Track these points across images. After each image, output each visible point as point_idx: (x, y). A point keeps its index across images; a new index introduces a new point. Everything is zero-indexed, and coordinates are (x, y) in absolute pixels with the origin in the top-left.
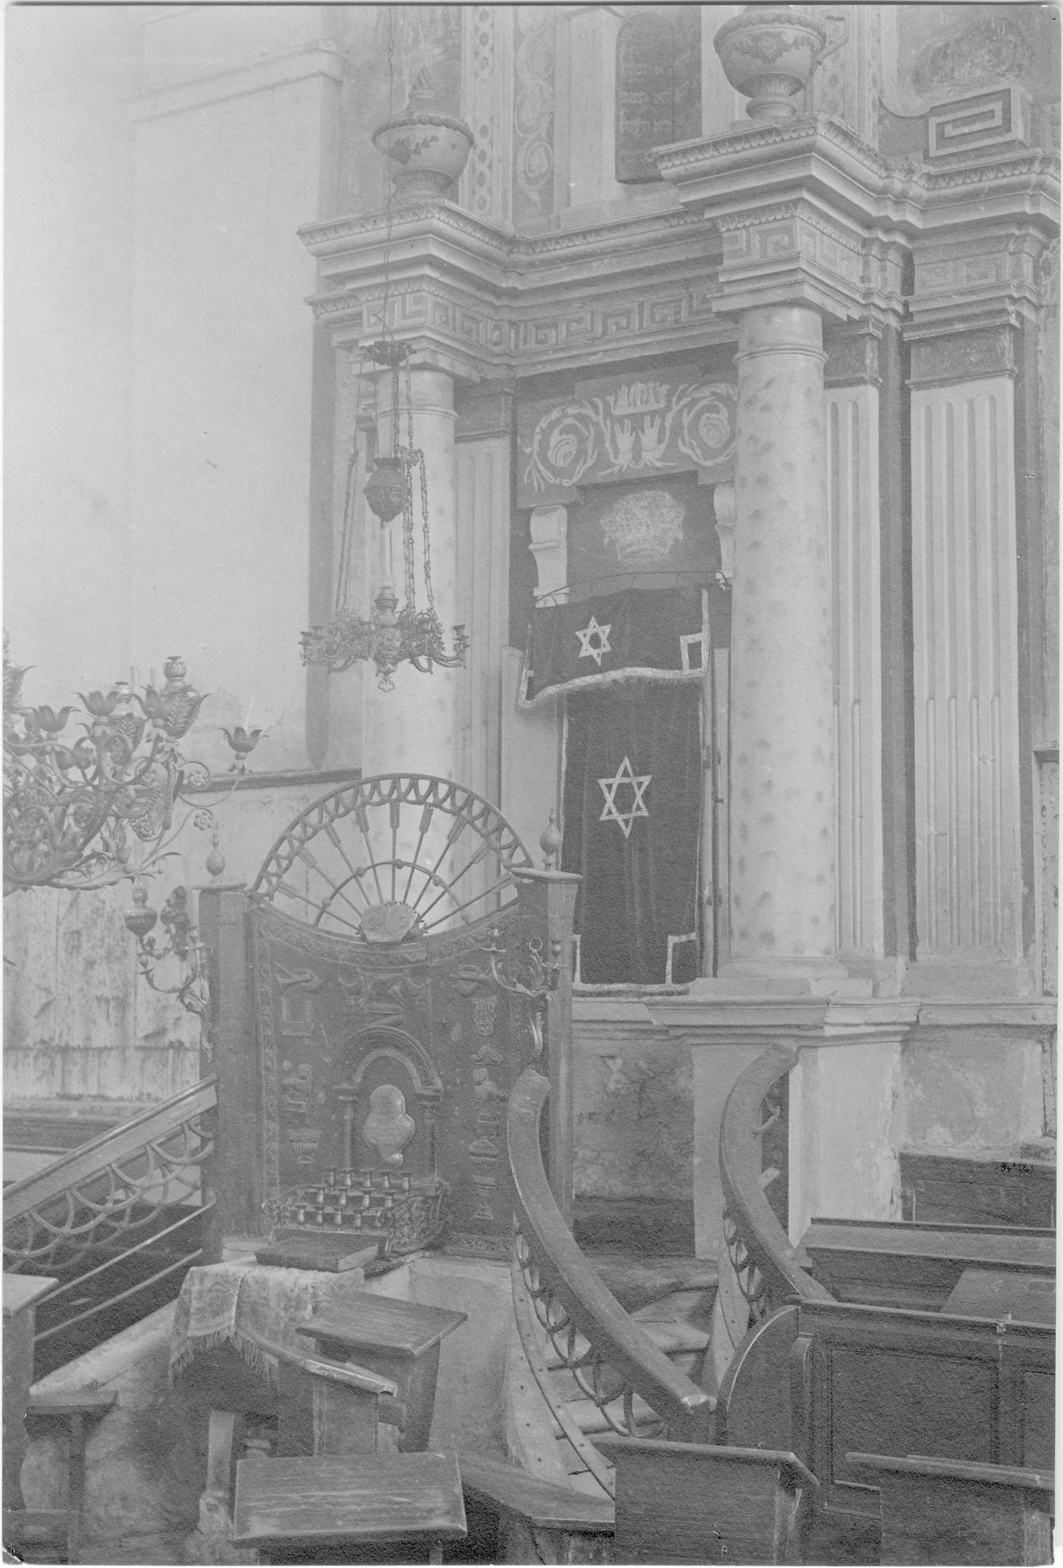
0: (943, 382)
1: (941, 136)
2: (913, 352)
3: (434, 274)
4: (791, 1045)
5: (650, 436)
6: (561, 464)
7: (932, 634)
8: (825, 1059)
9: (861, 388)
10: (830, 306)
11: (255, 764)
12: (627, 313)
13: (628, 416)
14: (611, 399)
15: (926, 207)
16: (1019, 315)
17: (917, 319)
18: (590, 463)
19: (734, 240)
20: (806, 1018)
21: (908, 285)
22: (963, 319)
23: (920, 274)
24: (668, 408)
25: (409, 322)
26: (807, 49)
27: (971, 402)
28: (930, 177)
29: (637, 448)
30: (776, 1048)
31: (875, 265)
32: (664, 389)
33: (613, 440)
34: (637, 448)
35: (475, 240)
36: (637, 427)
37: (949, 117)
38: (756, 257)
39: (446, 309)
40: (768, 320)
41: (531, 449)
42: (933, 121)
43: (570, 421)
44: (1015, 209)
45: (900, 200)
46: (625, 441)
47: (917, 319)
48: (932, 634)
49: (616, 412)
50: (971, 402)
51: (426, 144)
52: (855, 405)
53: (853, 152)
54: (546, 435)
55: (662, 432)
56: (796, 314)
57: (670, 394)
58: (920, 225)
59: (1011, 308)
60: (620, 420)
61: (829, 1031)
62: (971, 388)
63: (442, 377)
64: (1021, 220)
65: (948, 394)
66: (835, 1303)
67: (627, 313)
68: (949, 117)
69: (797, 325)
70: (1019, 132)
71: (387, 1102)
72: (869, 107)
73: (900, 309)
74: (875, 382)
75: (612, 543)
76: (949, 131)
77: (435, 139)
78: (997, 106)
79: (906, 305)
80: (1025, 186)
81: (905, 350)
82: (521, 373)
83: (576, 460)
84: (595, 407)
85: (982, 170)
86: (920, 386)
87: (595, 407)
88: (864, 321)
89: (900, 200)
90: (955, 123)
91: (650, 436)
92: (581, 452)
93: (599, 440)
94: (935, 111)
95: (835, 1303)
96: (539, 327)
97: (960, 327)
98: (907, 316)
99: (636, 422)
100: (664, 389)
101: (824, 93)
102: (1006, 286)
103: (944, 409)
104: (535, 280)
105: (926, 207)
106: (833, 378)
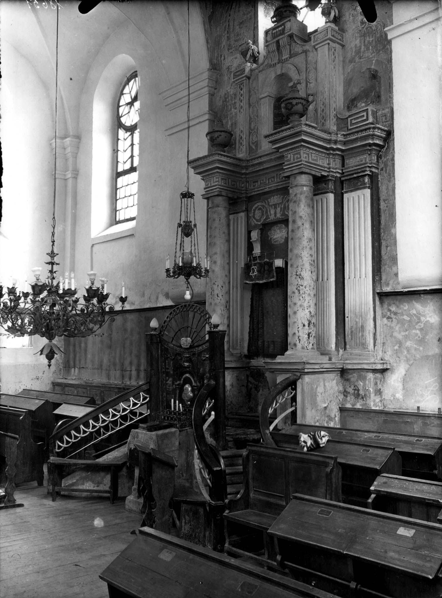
0: (351, 191)
1: (351, 122)
2: (344, 182)
3: (218, 171)
4: (299, 374)
5: (278, 210)
6: (258, 218)
7: (349, 261)
8: (307, 379)
9: (328, 194)
10: (313, 173)
11: (127, 307)
12: (274, 177)
13: (273, 205)
14: (269, 200)
15: (345, 143)
16: (371, 171)
17: (345, 174)
18: (264, 218)
19: (287, 157)
20: (300, 367)
21: (343, 165)
22: (355, 173)
23: (347, 161)
24: (283, 202)
25: (215, 184)
26: (300, 105)
27: (359, 196)
28: (344, 135)
29: (275, 213)
30: (295, 375)
31: (332, 161)
32: (282, 196)
33: (270, 211)
34: (275, 213)
35: (234, 162)
36: (275, 208)
37: (353, 118)
38: (292, 161)
39: (226, 180)
40: (295, 178)
41: (251, 215)
42: (349, 119)
43: (260, 207)
44: (367, 142)
45: (336, 142)
46: (272, 212)
47: (345, 174)
48: (349, 261)
49: (270, 204)
50: (359, 196)
51: (218, 137)
52: (327, 199)
53: (317, 131)
54: (255, 210)
55: (281, 209)
56: (303, 176)
57: (283, 198)
58: (344, 148)
59: (368, 169)
60: (271, 206)
61: (306, 371)
62: (359, 192)
63: (224, 198)
64: (370, 145)
65: (353, 194)
66: (276, 447)
67: (274, 177)
68: (353, 118)
69: (304, 180)
70: (371, 120)
71: (187, 389)
72: (332, 117)
73: (340, 171)
74: (369, 188)
75: (271, 239)
76: (353, 122)
77: (220, 135)
78: (365, 114)
79: (342, 170)
80: (369, 135)
81: (342, 182)
82: (249, 195)
83: (261, 218)
84: (265, 203)
85: (357, 132)
86: (346, 192)
87: (265, 203)
88: (328, 176)
89: (336, 142)
90: (355, 119)
91: (278, 210)
92: (263, 214)
93: (267, 212)
94: (350, 116)
95: (276, 447)
96: (254, 182)
97: (355, 176)
98: (343, 173)
99: (275, 206)
100: (282, 196)
101: (321, 114)
102: (366, 163)
103: (352, 199)
104: (251, 170)
105: (345, 143)
106: (316, 193)
